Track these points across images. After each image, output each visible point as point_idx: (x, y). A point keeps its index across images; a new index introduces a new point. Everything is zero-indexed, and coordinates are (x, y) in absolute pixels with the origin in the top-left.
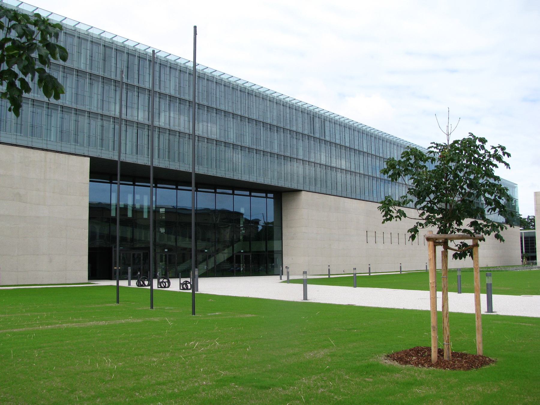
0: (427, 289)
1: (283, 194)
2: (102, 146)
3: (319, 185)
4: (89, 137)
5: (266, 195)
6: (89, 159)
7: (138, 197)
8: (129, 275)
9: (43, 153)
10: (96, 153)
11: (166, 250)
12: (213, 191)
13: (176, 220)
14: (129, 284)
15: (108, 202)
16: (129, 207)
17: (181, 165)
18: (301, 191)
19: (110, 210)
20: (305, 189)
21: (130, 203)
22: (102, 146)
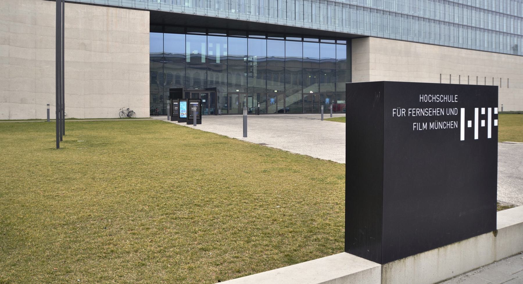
0: (166, 115)
1: (353, 41)
2: (269, 15)
3: (442, 39)
4: (454, 37)
5: (336, 42)
6: (149, 12)
7: (179, 44)
8: (322, 111)
9: (105, 8)
10: (155, 8)
11: (276, 91)
12: (283, 38)
13: (268, 68)
14: (331, 116)
15: (183, 52)
16: (187, 57)
17: (149, 4)
18: (368, 37)
19: (185, 59)
20: (372, 35)
21: (203, 53)
22: (269, 15)
